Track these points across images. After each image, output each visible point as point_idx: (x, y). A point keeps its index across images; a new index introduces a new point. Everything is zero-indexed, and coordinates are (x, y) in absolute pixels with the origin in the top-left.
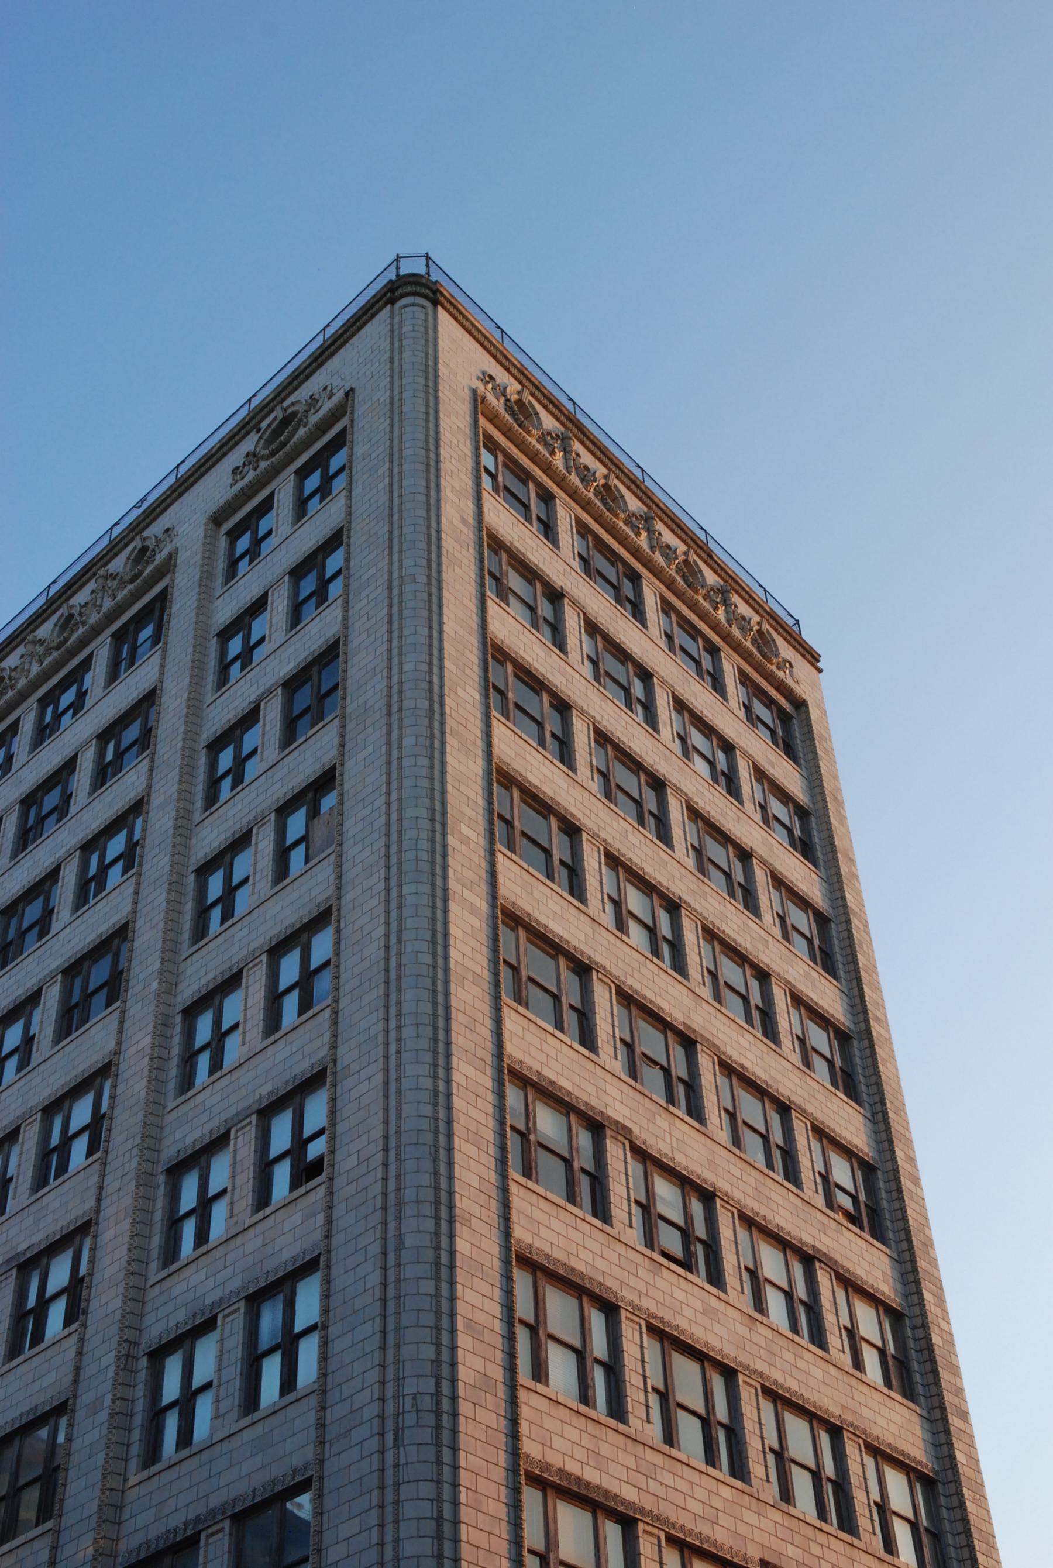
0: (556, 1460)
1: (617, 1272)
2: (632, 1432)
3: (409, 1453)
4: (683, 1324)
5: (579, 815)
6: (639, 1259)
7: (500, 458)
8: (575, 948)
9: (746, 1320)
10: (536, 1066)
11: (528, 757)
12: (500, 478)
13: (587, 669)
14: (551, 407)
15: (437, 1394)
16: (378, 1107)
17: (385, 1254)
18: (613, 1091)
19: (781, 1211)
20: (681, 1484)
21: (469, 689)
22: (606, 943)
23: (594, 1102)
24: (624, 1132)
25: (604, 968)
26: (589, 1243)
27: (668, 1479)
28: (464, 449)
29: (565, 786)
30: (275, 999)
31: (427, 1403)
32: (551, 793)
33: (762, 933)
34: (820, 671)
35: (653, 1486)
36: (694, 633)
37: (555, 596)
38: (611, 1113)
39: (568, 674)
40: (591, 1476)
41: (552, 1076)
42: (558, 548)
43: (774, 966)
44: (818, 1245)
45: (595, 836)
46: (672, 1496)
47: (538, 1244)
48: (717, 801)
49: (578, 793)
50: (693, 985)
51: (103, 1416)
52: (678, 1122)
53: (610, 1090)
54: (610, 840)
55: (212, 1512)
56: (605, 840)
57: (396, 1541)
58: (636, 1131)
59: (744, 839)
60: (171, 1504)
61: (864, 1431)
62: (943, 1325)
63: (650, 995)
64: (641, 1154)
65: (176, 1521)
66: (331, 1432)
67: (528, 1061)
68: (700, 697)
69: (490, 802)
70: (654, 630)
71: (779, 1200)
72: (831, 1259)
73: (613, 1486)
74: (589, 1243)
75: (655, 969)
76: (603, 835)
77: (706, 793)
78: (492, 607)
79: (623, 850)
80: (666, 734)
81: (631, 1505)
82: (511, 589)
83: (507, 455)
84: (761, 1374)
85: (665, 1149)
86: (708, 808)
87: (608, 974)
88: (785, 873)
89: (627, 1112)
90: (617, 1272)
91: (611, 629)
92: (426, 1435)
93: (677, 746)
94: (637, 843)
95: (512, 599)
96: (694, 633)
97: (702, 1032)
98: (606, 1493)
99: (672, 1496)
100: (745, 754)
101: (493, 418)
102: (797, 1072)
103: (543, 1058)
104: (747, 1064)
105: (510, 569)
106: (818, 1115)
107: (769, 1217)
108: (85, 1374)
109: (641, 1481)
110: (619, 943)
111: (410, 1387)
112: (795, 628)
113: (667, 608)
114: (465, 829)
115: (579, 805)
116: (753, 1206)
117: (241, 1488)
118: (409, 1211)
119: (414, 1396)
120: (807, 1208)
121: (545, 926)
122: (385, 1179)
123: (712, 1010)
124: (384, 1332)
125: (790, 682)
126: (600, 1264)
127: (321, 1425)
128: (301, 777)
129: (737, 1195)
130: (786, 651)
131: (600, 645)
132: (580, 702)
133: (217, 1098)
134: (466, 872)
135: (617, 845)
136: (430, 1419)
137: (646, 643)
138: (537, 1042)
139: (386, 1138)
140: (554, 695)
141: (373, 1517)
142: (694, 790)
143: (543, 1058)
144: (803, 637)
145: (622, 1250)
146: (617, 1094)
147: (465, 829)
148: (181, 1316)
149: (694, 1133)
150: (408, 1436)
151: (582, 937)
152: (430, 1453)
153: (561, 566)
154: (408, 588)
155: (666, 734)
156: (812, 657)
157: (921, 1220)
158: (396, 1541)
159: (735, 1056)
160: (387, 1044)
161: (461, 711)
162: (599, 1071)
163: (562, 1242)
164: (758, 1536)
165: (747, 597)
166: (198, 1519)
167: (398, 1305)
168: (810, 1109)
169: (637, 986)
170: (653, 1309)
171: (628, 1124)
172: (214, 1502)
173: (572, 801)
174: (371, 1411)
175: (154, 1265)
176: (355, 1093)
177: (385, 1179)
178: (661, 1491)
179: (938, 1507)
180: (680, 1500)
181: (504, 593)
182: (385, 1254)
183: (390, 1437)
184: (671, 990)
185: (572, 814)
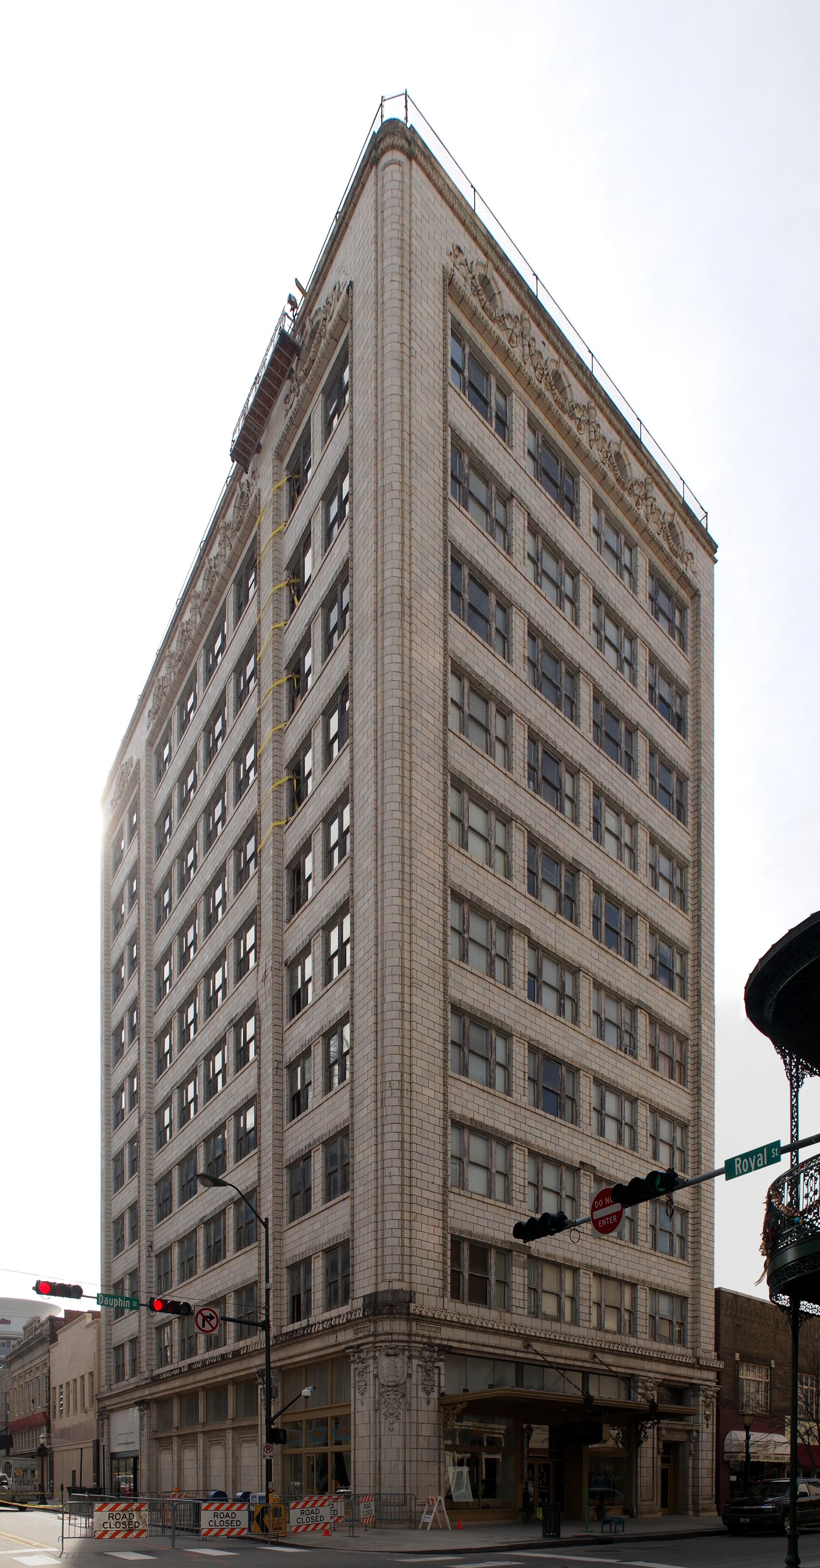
0: (469, 1114)
1: (512, 1015)
2: (514, 1101)
3: (388, 1111)
4: (551, 1044)
5: (511, 700)
6: (528, 1008)
7: (467, 350)
8: (502, 805)
9: (590, 1042)
10: (470, 889)
11: (476, 652)
12: (466, 373)
13: (529, 569)
14: (513, 283)
15: (402, 1081)
16: (372, 919)
17: (376, 1006)
18: (520, 905)
19: (622, 979)
20: (539, 1126)
21: (431, 592)
22: (523, 801)
23: (507, 912)
24: (525, 931)
25: (521, 819)
26: (497, 999)
27: (533, 1124)
28: (433, 340)
29: (502, 676)
30: (328, 853)
31: (396, 1085)
32: (491, 682)
33: (637, 790)
34: (715, 561)
35: (523, 1127)
36: (618, 530)
37: (507, 497)
38: (518, 919)
39: (511, 574)
40: (489, 1122)
41: (480, 896)
42: (511, 447)
43: (641, 816)
44: (641, 999)
45: (522, 717)
46: (534, 1131)
47: (465, 999)
48: (618, 685)
49: (512, 682)
50: (582, 830)
51: (270, 1098)
52: (561, 925)
53: (518, 904)
54: (533, 720)
55: (315, 1141)
56: (529, 720)
57: (383, 1151)
58: (533, 930)
59: (633, 715)
60: (300, 1139)
61: (651, 1100)
62: (710, 1044)
63: (551, 838)
64: (534, 945)
65: (302, 1146)
66: (356, 1101)
67: (465, 885)
68: (615, 590)
69: (445, 691)
70: (586, 529)
71: (621, 972)
72: (647, 1006)
73: (501, 1127)
74: (497, 999)
75: (556, 819)
76: (528, 715)
77: (610, 678)
78: (453, 512)
79: (542, 728)
80: (585, 626)
81: (509, 1135)
82: (470, 493)
83: (473, 346)
84: (594, 1071)
85: (551, 941)
86: (609, 691)
87: (523, 823)
88: (660, 742)
89: (528, 918)
90: (512, 1015)
91: (550, 529)
92: (396, 1101)
93: (592, 638)
94: (553, 721)
95: (471, 503)
96: (618, 530)
97: (584, 863)
98: (497, 1130)
99: (534, 1131)
100: (645, 643)
101: (461, 301)
102: (646, 890)
103: (475, 883)
104: (613, 885)
105: (471, 473)
106: (656, 919)
107: (613, 982)
108: (262, 1078)
109: (517, 1125)
110: (533, 800)
111: (388, 1077)
112: (703, 523)
113: (598, 504)
114: (425, 714)
115: (512, 692)
116: (604, 976)
117: (324, 1131)
118: (388, 981)
119: (390, 1082)
120: (638, 977)
121: (482, 789)
122: (376, 963)
123: (593, 848)
124: (376, 1049)
125: (689, 574)
126: (503, 1010)
127: (352, 1098)
128: (333, 684)
129: (594, 970)
130: (689, 542)
131: (540, 545)
132: (519, 601)
133: (304, 922)
134: (425, 748)
135: (538, 724)
136: (398, 1093)
137: (575, 541)
138: (471, 872)
139: (376, 937)
140: (500, 594)
141: (373, 1141)
142: (600, 675)
143: (475, 883)
144: (709, 531)
145: (517, 1002)
146: (523, 907)
147: (425, 714)
148: (297, 1047)
149: (571, 931)
150: (388, 1102)
151: (507, 796)
152: (398, 1110)
153: (512, 467)
154: (389, 496)
155: (585, 626)
156: (711, 547)
157: (709, 983)
158: (383, 1151)
159: (605, 880)
160: (376, 877)
161: (424, 612)
162: (512, 892)
163: (480, 998)
164: (580, 1150)
165: (665, 489)
166: (310, 1145)
167: (383, 1034)
168: (650, 914)
169: (543, 832)
170: (533, 1036)
171: (528, 926)
172: (316, 1137)
173: (507, 688)
174: (372, 1089)
175: (285, 1021)
176: (362, 911)
177: (376, 963)
178: (528, 1130)
179: (687, 1137)
180: (538, 1133)
181: (466, 497)
182: (376, 1006)
183: (379, 1103)
184: (566, 834)
185: (507, 700)
